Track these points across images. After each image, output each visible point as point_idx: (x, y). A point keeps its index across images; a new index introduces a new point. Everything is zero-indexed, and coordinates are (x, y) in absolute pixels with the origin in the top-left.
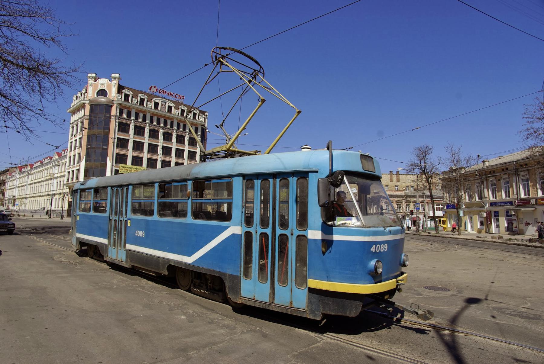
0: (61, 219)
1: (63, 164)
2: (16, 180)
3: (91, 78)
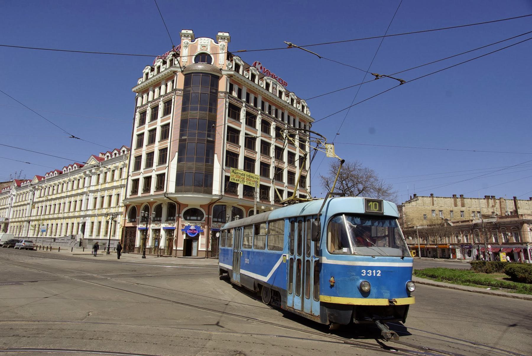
0: (143, 257)
1: (61, 184)
2: (10, 199)
3: (187, 36)
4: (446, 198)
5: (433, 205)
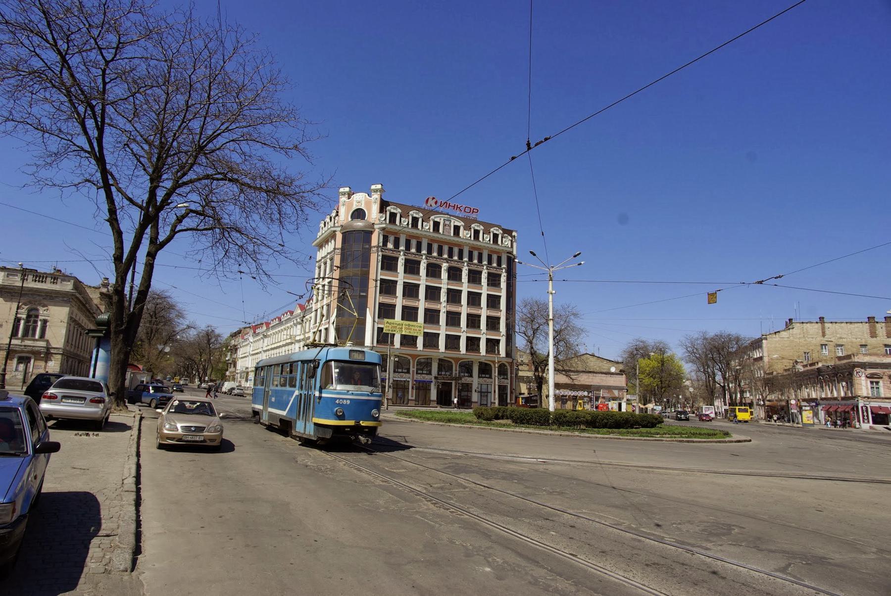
3: (344, 194)
4: (851, 323)
5: (824, 335)
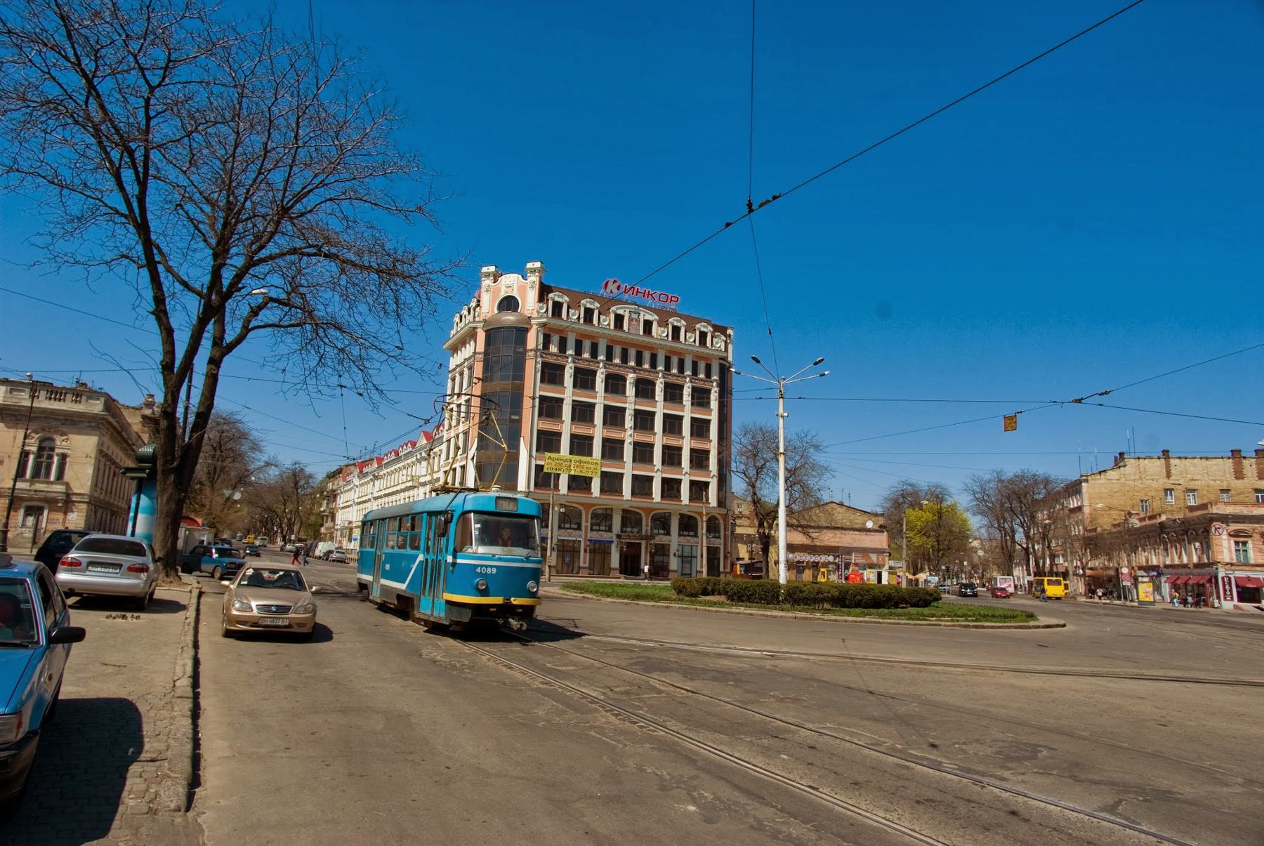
3: (488, 275)
5: (1169, 475)
